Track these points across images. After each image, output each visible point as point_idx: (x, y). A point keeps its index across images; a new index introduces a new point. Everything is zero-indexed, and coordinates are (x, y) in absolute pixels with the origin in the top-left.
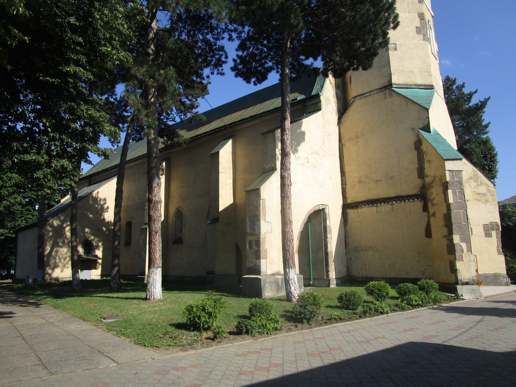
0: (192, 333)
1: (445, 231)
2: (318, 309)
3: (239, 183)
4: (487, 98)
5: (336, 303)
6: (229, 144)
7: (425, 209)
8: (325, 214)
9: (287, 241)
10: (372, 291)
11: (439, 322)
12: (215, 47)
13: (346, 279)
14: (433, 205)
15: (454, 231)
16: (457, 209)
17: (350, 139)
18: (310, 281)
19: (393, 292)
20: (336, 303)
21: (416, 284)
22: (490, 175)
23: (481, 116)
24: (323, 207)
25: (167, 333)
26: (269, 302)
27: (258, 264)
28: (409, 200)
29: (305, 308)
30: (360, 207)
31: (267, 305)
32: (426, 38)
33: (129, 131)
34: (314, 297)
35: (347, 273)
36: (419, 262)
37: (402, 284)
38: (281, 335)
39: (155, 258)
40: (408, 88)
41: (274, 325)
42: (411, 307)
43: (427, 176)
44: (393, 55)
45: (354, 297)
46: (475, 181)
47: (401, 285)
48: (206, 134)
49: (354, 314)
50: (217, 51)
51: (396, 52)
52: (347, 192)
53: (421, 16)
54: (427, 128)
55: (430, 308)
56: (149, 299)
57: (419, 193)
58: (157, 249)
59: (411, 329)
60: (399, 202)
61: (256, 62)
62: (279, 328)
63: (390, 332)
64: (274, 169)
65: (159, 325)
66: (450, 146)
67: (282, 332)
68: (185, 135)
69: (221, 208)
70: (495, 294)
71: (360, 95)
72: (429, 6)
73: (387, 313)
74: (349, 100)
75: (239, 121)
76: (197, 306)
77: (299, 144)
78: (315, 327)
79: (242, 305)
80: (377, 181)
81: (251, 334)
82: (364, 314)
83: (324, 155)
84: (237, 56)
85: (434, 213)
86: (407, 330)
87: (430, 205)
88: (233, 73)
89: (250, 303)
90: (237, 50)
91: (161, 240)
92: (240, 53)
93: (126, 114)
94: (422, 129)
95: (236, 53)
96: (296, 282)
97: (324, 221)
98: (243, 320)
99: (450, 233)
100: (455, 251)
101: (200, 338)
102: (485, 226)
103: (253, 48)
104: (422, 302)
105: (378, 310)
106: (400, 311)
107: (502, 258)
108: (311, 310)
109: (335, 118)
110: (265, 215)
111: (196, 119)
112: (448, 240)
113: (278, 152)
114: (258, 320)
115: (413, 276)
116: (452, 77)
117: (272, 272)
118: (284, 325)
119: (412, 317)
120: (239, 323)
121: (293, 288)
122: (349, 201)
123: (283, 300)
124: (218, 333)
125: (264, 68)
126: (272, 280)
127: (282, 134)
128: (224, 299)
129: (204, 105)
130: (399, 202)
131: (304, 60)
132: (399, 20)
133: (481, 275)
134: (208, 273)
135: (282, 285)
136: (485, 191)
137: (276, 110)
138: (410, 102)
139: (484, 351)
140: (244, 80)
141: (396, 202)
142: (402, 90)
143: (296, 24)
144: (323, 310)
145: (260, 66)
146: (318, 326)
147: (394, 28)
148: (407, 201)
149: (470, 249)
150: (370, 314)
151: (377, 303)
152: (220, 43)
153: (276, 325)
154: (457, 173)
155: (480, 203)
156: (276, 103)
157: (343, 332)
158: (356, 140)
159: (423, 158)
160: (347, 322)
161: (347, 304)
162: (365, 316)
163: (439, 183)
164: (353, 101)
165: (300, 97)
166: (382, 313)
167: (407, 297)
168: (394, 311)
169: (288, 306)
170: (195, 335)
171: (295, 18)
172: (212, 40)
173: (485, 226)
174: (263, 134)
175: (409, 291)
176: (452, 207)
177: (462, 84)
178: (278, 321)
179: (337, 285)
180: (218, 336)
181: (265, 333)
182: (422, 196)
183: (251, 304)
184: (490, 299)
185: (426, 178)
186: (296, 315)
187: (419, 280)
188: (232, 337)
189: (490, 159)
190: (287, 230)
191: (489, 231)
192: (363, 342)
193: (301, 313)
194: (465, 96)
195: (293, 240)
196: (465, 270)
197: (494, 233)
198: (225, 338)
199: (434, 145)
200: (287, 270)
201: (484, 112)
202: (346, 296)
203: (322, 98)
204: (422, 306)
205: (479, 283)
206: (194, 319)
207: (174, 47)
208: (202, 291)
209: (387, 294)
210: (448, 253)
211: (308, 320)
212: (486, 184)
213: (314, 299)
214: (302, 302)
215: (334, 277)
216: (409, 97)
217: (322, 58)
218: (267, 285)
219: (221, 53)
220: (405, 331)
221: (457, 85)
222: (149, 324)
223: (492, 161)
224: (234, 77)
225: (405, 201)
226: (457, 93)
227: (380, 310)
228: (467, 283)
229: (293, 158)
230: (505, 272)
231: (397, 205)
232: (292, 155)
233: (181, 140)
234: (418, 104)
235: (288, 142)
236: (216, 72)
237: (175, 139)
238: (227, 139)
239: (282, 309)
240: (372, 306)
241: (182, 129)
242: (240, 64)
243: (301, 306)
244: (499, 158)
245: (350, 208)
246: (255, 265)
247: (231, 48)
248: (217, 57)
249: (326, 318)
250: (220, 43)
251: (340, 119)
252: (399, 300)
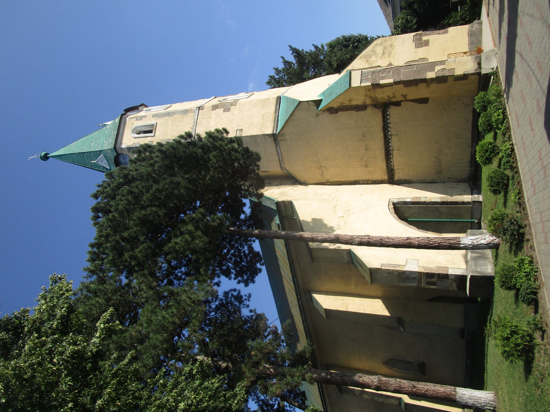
0: (537, 355)
1: (422, 86)
2: (508, 216)
3: (361, 291)
4: (289, 48)
5: (501, 196)
6: (317, 296)
7: (397, 104)
8: (398, 203)
9: (429, 244)
10: (487, 159)
11: (523, 95)
12: (224, 301)
13: (474, 184)
14: (394, 97)
15: (423, 78)
16: (399, 75)
17: (322, 174)
18: (474, 222)
19: (489, 138)
20: (501, 196)
21: (479, 114)
22: (364, 42)
23: (306, 52)
25: (536, 384)
26: (498, 267)
27: (454, 277)
28: (388, 119)
29: (507, 230)
30: (392, 167)
31: (503, 270)
32: (234, 103)
33: (296, 404)
34: (494, 219)
35: (465, 182)
36: (454, 110)
37: (480, 128)
38: (538, 257)
39: (444, 392)
40: (278, 120)
41: (526, 264)
42: (506, 120)
43: (365, 102)
44: (246, 133)
45: (494, 178)
46: (370, 57)
47: (480, 129)
48: (304, 321)
49: (513, 178)
50: (228, 299)
52: (376, 179)
53: (215, 107)
54: (318, 103)
55: (507, 102)
56: (495, 407)
57: (381, 109)
58: (433, 388)
59: (531, 123)
60: (389, 129)
61: (242, 261)
62: (529, 259)
63: (533, 145)
64: (349, 252)
65: (527, 394)
66: (337, 83)
67: (534, 256)
68: (302, 344)
69: (386, 313)
70: (491, 36)
71: (280, 163)
72: (206, 100)
73: (512, 144)
74: (284, 174)
75: (294, 284)
76: (504, 346)
77: (325, 225)
78: (529, 220)
79: (503, 298)
80: (366, 149)
81: (537, 289)
82: (514, 168)
84: (235, 279)
86: (532, 127)
87: (394, 100)
88: (251, 285)
89: (500, 289)
90: (230, 279)
91: (423, 383)
92: (233, 276)
93: (276, 407)
94: (318, 106)
95: (232, 280)
96: (476, 237)
97: (406, 205)
98: (520, 296)
99: (425, 81)
100: (443, 76)
101: (543, 347)
102: (417, 46)
103: (230, 263)
104: (501, 109)
105: (509, 154)
106: (510, 131)
107: (451, 29)
108: (509, 224)
109: (300, 188)
110: (399, 266)
111: (288, 330)
112: (431, 83)
113: (332, 246)
114: (521, 281)
115: (470, 116)
116: (267, 79)
117: (464, 263)
118: (526, 253)
119: (518, 121)
120: (523, 301)
121: (483, 242)
122: (386, 177)
123: (497, 253)
124: (536, 325)
125: (249, 254)
126: (473, 264)
127: (317, 241)
128: (495, 317)
129: (273, 319)
130: (389, 129)
131: (246, 215)
132: (221, 129)
133: (470, 48)
134: (463, 337)
135: (479, 253)
136: (381, 47)
137: (287, 246)
139: (494, 295)
140: (257, 275)
141: (389, 131)
142: (279, 125)
143: (218, 221)
144: (508, 211)
145: (246, 258)
146: (528, 217)
147: (227, 133)
148: (389, 121)
149: (442, 62)
150: (513, 162)
151: (501, 154)
152: (221, 295)
153: (526, 262)
154: (363, 75)
155: (393, 52)
156: (279, 246)
157: (535, 192)
158: (323, 168)
159: (346, 106)
160: (523, 186)
161: (502, 185)
162: (516, 167)
163: (372, 92)
164: (285, 170)
165: (277, 220)
166: (513, 150)
167: (494, 124)
168: (510, 137)
169: (504, 248)
170: (539, 352)
171: (214, 222)
172: (217, 303)
173: (417, 46)
174: (312, 260)
175: (488, 121)
176: (398, 79)
177: (275, 70)
178: (522, 259)
179: (479, 193)
180: (539, 326)
181: (536, 274)
182: (384, 107)
183: (502, 287)
184: (497, 42)
185: (367, 104)
186: (515, 239)
187: (474, 110)
188: (540, 311)
189: (348, 41)
190: (417, 243)
191: (422, 43)
192: (545, 173)
193: (512, 234)
194: (286, 67)
195: (428, 238)
196: (465, 66)
197: (424, 38)
198: (541, 318)
199: (334, 96)
200: (461, 246)
201: (303, 50)
202: (492, 186)
203: (280, 200)
204: (505, 109)
205: (480, 51)
206: (519, 351)
207: (217, 343)
208: (484, 345)
209: (490, 143)
210: (427, 103)
211: (520, 227)
212: (374, 47)
213: (496, 219)
214: (500, 232)
215: (470, 196)
216: (286, 119)
217: (245, 198)
218: (479, 270)
219: (230, 296)
220: (532, 129)
221: (275, 75)
222: (526, 405)
223: (350, 40)
224: (255, 284)
225: (388, 123)
226: (283, 74)
227: (509, 152)
228: (479, 64)
229: (342, 231)
230: (467, 26)
231: (392, 131)
232: (335, 233)
233: (309, 349)
234: (294, 110)
235: (325, 236)
236: (247, 303)
237: (307, 356)
238: (312, 299)
239: (508, 255)
240: (504, 160)
241: (296, 347)
242: (242, 277)
243: (505, 234)
244: (347, 34)
245: (394, 177)
246: (455, 281)
247: (226, 284)
248: (233, 300)
249: (518, 209)
250: (221, 295)
251: (301, 183)
252: (498, 131)
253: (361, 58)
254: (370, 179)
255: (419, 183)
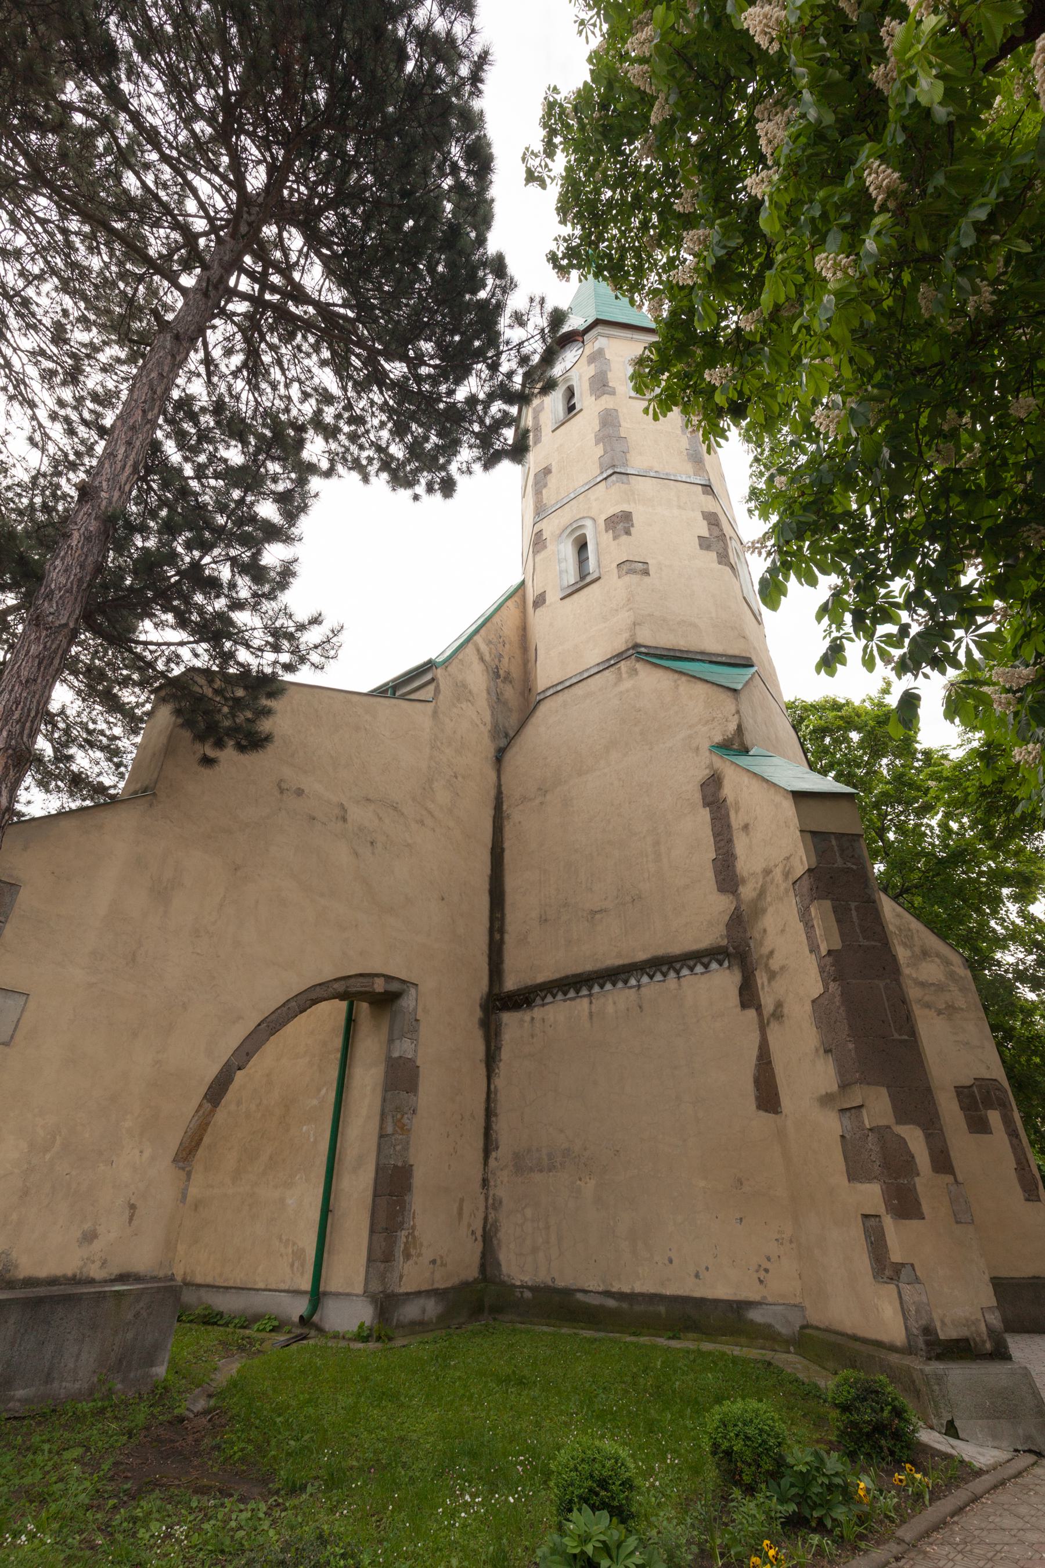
7: (748, 995)
14: (772, 976)
24: (394, 987)
28: (692, 969)
30: (538, 1001)
35: (483, 1267)
51: (646, 579)
57: (725, 942)
83: (422, 822)
85: (779, 1005)
87: (761, 978)
122: (511, 983)
138: (684, 679)
141: (651, 977)
148: (685, 972)
163: (783, 886)
191: (977, 1109)
210: (759, 1107)
212: (938, 955)
225: (678, 972)
253: (898, 915)
254: (506, 937)
255: (488, 1092)
